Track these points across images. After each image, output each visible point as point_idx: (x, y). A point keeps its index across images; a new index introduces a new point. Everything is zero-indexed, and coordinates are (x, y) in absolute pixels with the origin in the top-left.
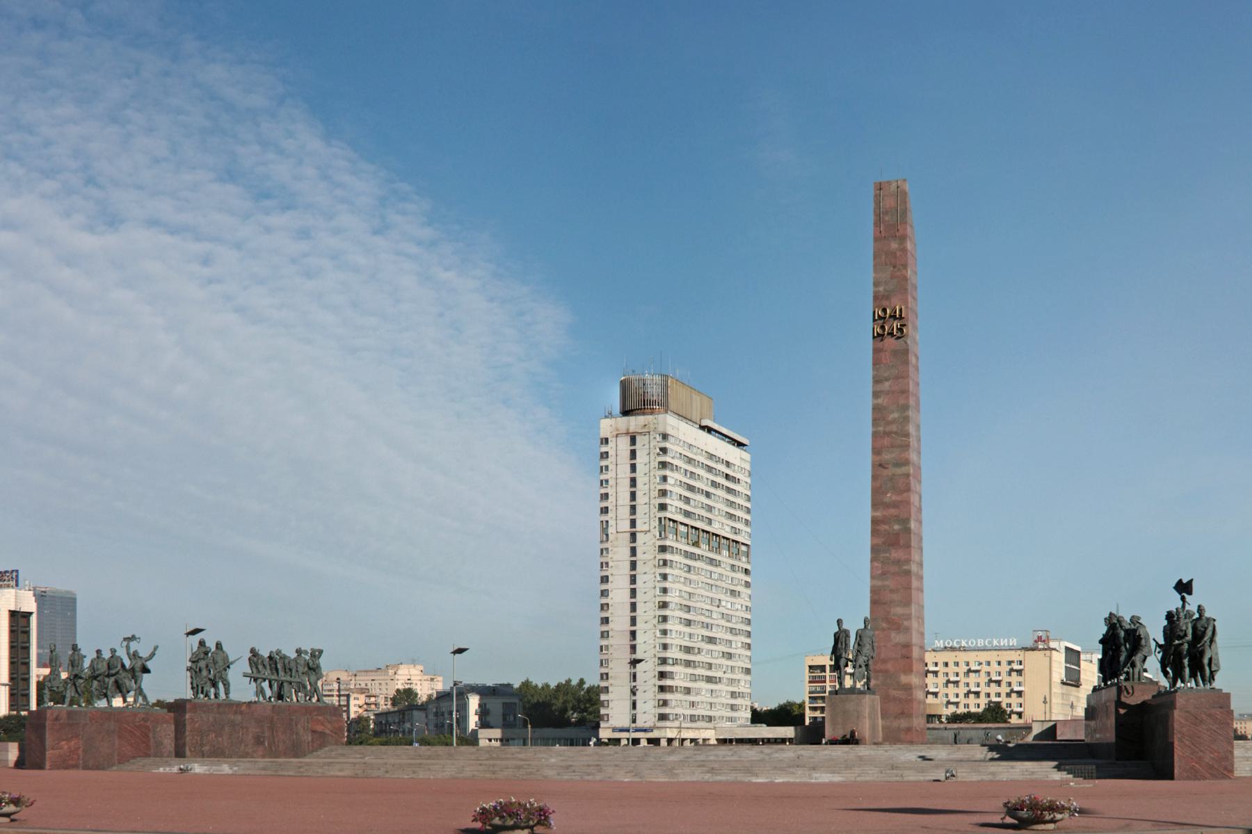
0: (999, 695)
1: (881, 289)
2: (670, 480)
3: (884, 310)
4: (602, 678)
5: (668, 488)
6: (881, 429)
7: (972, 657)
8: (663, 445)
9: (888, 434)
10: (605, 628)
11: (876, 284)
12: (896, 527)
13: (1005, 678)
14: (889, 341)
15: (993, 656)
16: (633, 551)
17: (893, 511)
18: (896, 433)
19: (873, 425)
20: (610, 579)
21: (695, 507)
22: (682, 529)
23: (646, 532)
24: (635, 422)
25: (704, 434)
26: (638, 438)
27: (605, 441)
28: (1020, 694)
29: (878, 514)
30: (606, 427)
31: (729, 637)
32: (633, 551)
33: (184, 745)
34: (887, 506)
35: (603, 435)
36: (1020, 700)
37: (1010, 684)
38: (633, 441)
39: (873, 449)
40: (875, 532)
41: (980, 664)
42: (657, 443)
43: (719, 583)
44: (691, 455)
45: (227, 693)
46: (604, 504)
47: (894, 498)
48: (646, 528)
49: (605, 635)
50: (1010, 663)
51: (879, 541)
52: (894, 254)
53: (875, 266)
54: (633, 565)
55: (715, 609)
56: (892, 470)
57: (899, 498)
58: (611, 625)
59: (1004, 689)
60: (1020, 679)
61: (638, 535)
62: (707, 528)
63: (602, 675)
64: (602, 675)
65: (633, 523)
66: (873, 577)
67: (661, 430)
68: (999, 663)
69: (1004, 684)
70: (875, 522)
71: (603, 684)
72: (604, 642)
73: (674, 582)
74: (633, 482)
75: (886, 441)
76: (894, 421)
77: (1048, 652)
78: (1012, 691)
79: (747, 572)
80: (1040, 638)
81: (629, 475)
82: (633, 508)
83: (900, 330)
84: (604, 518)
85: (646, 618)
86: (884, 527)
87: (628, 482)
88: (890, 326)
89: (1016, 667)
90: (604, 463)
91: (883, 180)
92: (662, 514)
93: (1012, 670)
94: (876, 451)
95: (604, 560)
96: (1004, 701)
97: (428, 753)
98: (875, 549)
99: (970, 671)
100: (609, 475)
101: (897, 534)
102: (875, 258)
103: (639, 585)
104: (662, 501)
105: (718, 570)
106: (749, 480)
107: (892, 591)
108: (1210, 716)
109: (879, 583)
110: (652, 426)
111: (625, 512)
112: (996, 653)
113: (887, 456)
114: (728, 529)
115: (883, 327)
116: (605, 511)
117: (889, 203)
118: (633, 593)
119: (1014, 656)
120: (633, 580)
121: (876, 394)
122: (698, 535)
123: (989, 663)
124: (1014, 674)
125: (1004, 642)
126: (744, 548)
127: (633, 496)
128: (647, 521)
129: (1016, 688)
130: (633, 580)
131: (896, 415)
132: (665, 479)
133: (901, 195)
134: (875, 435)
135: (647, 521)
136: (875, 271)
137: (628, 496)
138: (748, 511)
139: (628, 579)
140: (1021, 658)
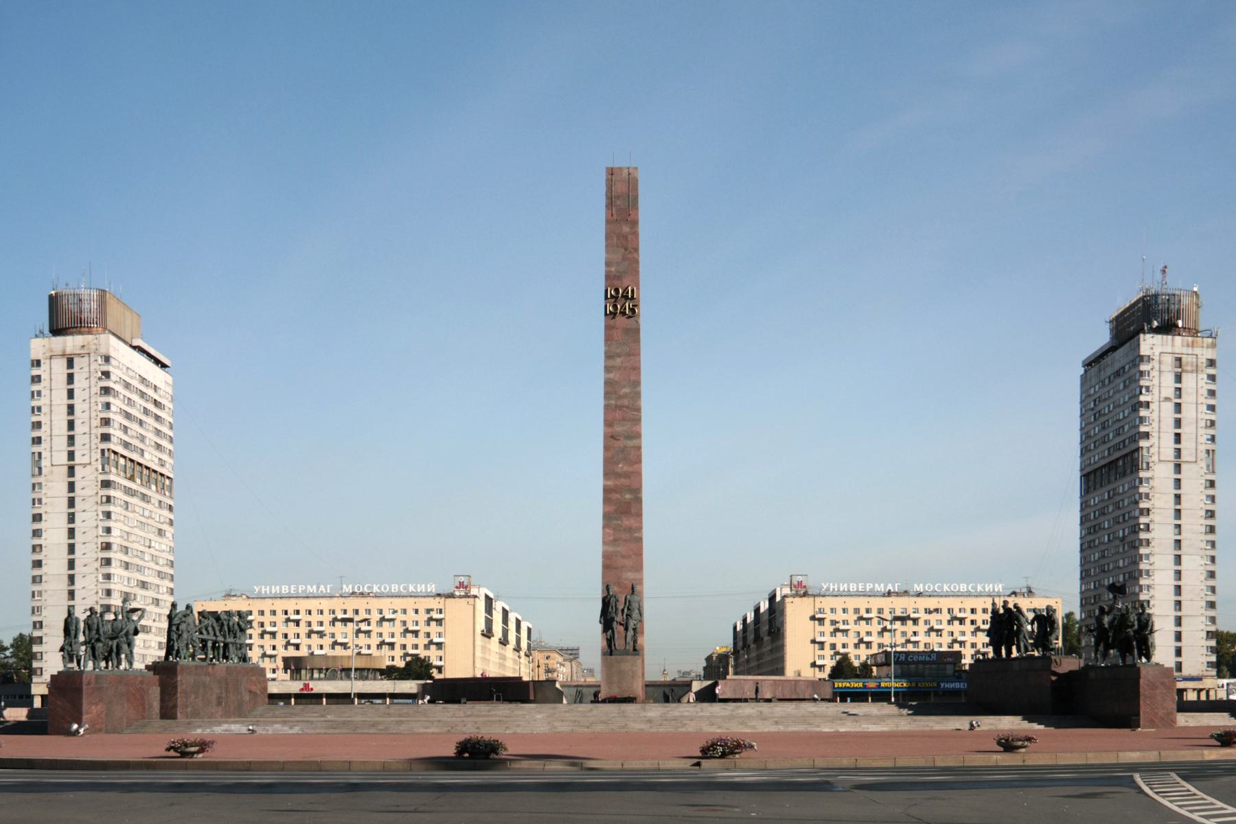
0: (416, 647)
1: (613, 269)
2: (113, 408)
3: (617, 290)
4: (35, 627)
5: (111, 416)
6: (613, 402)
7: (386, 605)
8: (105, 368)
9: (620, 407)
10: (37, 572)
11: (608, 264)
12: (628, 496)
13: (423, 628)
14: (620, 319)
15: (409, 604)
16: (71, 487)
17: (623, 481)
18: (627, 407)
19: (605, 398)
20: (44, 517)
21: (132, 437)
22: (122, 461)
23: (85, 465)
24: (71, 343)
25: (135, 354)
26: (76, 361)
27: (37, 363)
28: (439, 646)
29: (609, 483)
30: (40, 346)
31: (157, 581)
32: (71, 487)
33: (175, 706)
34: (619, 475)
35: (34, 356)
36: (440, 653)
37: (428, 635)
38: (70, 363)
39: (605, 420)
40: (606, 500)
41: (395, 612)
42: (98, 366)
43: (150, 521)
44: (128, 380)
45: (131, 664)
46: (36, 434)
47: (625, 468)
48: (86, 460)
49: (36, 580)
50: (428, 611)
51: (611, 508)
52: (626, 237)
53: (607, 246)
54: (71, 502)
55: (146, 550)
56: (623, 443)
57: (630, 469)
58: (44, 569)
59: (422, 641)
60: (440, 629)
61: (77, 468)
62: (141, 460)
63: (35, 623)
64: (35, 623)
65: (71, 455)
66: (605, 543)
67: (103, 351)
68: (417, 611)
69: (421, 635)
70: (607, 490)
71: (36, 634)
72: (36, 588)
73: (116, 521)
74: (71, 409)
75: (618, 414)
76: (625, 396)
77: (471, 600)
78: (431, 642)
79: (170, 508)
80: (461, 585)
81: (66, 401)
82: (71, 439)
83: (632, 310)
84: (36, 449)
85: (85, 561)
86: (616, 496)
87: (65, 410)
88: (621, 305)
89: (436, 616)
90: (35, 388)
91: (617, 165)
92: (105, 446)
93: (431, 619)
94: (608, 423)
95: (36, 496)
96: (422, 653)
97: (727, 713)
98: (607, 517)
99: (383, 619)
100: (42, 402)
101: (628, 503)
102: (607, 239)
103: (78, 525)
104: (105, 430)
105: (149, 507)
106: (170, 406)
107: (623, 557)
108: (1162, 683)
109: (610, 549)
110: (93, 347)
111: (61, 443)
112: (413, 600)
113: (618, 429)
114: (156, 461)
115: (615, 307)
116: (37, 441)
117: (620, 188)
118: (71, 533)
119: (435, 603)
120: (71, 518)
121: (608, 369)
122: (137, 469)
123: (405, 611)
124: (433, 623)
125: (421, 588)
126: (167, 482)
127: (71, 425)
128: (88, 450)
129: (436, 640)
130: (71, 518)
131: (626, 390)
132: (108, 406)
133: (632, 183)
134: (607, 407)
135: (88, 450)
136: (607, 251)
137: (65, 425)
138: (171, 440)
139: (65, 518)
140: (441, 606)
